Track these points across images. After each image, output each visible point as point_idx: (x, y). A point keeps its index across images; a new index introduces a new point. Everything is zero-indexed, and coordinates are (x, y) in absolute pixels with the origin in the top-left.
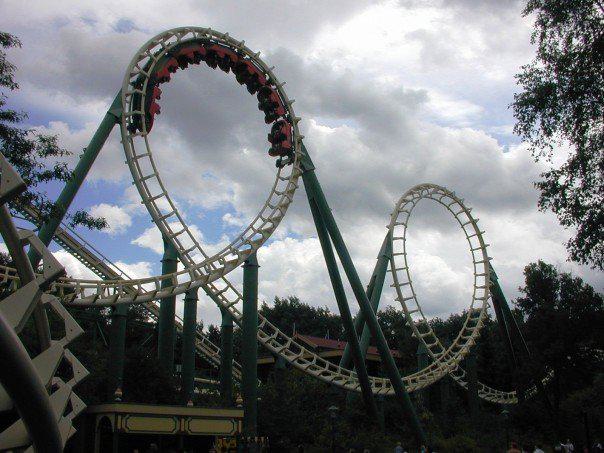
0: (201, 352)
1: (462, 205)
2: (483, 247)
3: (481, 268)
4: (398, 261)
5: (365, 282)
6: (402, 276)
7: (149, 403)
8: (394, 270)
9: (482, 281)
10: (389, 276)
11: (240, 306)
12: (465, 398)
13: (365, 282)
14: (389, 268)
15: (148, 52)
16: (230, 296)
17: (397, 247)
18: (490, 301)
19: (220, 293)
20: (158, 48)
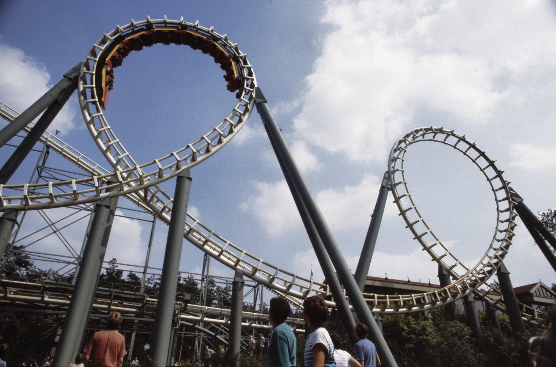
17: (397, 178)
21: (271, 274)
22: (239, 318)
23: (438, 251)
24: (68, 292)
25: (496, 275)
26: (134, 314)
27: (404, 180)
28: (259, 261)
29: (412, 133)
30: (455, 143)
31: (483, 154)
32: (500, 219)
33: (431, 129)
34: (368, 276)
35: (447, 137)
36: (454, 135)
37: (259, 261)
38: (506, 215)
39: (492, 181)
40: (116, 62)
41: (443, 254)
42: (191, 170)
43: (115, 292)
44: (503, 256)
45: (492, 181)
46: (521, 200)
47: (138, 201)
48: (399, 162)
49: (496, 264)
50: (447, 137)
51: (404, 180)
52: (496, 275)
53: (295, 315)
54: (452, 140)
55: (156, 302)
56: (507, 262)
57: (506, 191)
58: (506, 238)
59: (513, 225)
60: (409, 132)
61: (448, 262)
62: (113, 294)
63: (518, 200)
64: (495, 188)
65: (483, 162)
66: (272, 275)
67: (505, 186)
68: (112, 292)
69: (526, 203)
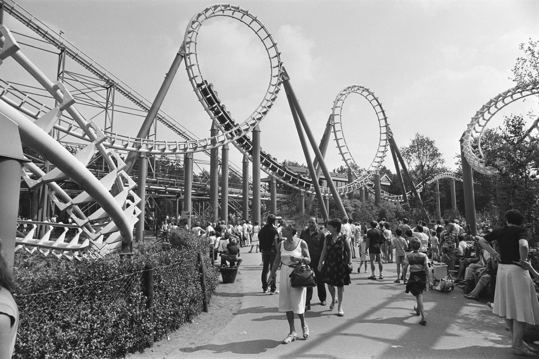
3: (384, 130)
4: (338, 127)
8: (335, 132)
9: (384, 137)
10: (332, 136)
14: (332, 130)
17: (337, 119)
22: (227, 192)
24: (437, 178)
28: (42, 105)
29: (358, 86)
31: (383, 112)
35: (368, 95)
36: (377, 101)
37: (42, 105)
38: (383, 149)
44: (259, 119)
46: (288, 79)
47: (28, 21)
48: (344, 96)
49: (253, 125)
50: (368, 95)
53: (527, 177)
55: (183, 182)
56: (262, 126)
57: (387, 128)
58: (266, 106)
59: (385, 155)
60: (356, 85)
65: (381, 116)
67: (387, 126)
69: (291, 82)
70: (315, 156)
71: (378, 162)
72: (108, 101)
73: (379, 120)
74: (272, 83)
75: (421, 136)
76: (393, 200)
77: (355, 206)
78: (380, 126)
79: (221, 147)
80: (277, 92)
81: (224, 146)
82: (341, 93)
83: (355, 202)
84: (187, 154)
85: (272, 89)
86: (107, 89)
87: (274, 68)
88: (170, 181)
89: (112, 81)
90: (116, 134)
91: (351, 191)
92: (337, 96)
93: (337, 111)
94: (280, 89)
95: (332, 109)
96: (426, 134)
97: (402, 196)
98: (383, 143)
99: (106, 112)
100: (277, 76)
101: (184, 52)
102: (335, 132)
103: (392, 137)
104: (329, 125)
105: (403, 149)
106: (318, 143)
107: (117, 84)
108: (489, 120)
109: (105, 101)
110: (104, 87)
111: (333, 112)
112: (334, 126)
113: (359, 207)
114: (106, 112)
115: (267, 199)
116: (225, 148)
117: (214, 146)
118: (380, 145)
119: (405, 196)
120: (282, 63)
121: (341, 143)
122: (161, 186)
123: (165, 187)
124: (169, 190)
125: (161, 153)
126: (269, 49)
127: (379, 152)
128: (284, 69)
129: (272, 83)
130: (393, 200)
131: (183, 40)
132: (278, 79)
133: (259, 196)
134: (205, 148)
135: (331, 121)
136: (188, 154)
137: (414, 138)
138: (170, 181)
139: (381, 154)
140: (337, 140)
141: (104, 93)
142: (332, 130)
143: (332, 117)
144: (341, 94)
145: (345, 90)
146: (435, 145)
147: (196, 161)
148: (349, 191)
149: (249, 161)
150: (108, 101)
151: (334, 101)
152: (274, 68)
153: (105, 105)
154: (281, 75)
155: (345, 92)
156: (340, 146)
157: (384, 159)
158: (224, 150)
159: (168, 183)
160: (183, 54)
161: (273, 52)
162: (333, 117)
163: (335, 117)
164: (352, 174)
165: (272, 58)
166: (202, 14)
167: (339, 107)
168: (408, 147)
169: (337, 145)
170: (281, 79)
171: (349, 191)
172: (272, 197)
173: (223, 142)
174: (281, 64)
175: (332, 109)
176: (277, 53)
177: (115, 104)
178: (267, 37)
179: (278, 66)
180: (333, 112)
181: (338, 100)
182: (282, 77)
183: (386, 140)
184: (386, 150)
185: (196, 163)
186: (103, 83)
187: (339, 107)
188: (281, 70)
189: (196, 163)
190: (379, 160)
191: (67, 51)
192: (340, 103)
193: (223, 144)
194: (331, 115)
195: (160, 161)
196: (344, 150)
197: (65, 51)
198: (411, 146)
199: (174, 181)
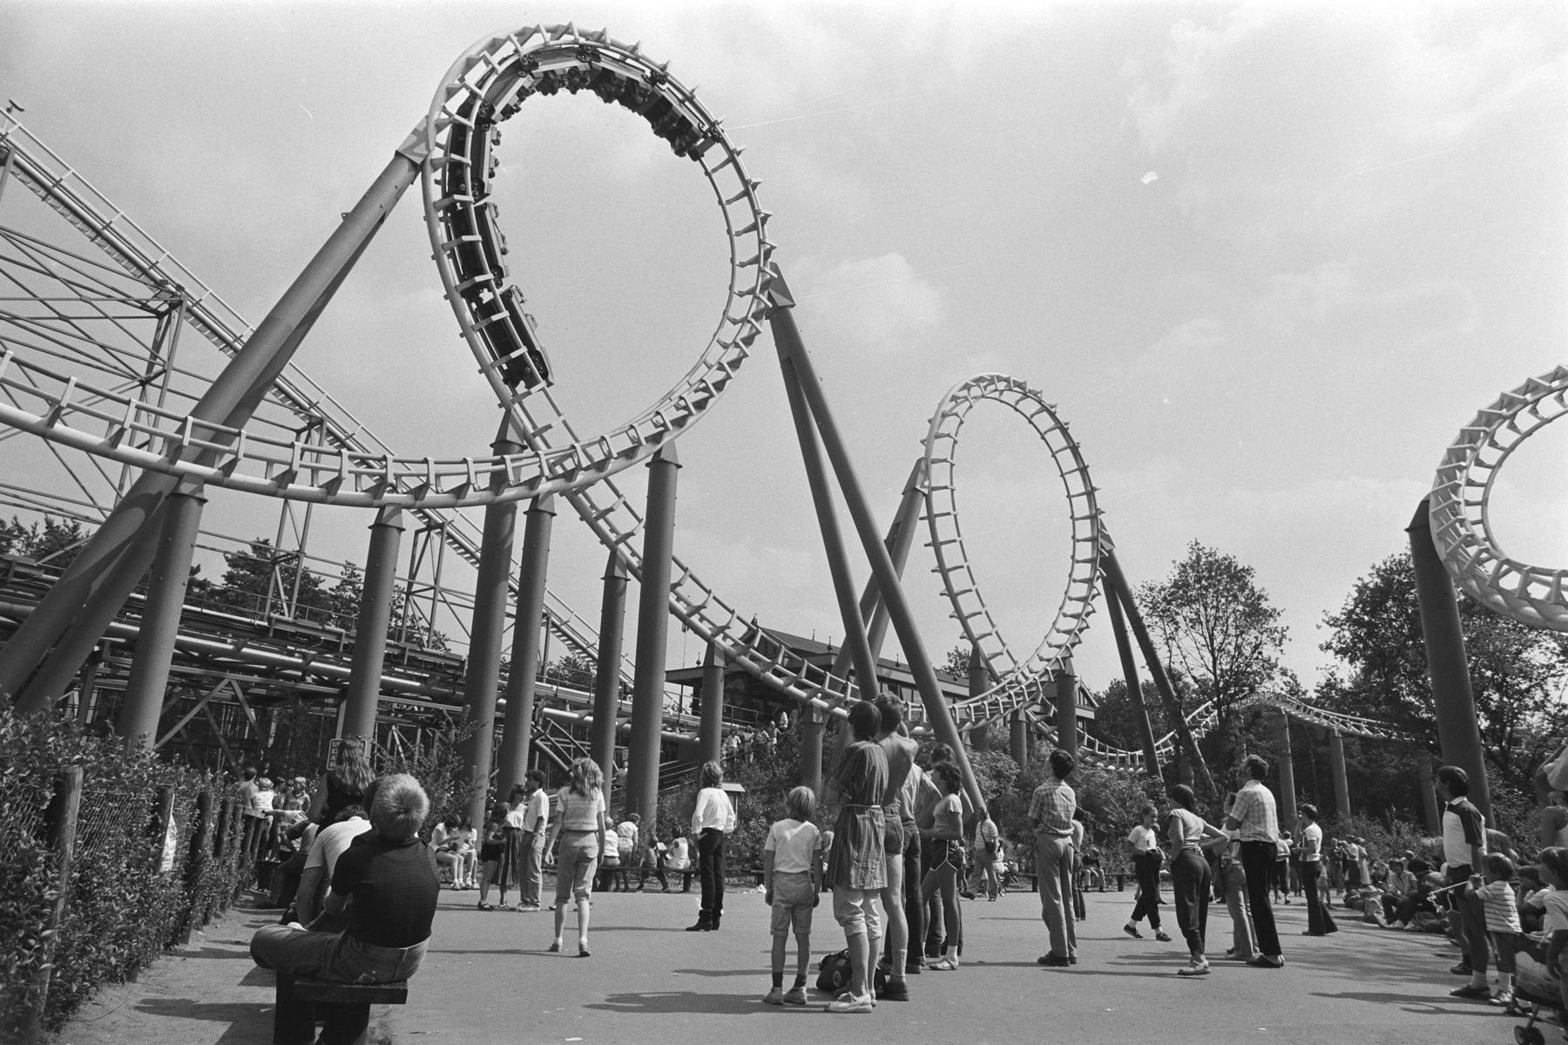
0: (1369, 944)
1: (1053, 415)
2: (1090, 493)
3: (1085, 530)
4: (940, 502)
5: (883, 527)
6: (945, 529)
7: (557, 709)
8: (931, 518)
9: (1085, 550)
10: (921, 531)
11: (638, 543)
12: (197, 720)
13: (883, 527)
14: (923, 512)
15: (462, 79)
16: (622, 521)
17: (939, 475)
18: (1099, 584)
19: (603, 514)
20: (480, 70)
21: (117, 418)
23: (978, 626)
25: (647, 465)
26: (417, 681)
27: (952, 484)
30: (1046, 429)
31: (1083, 470)
32: (1070, 594)
33: (1020, 385)
34: (881, 656)
38: (1082, 590)
39: (1076, 522)
40: (548, 85)
41: (987, 632)
42: (676, 440)
43: (410, 650)
45: (1076, 522)
50: (1021, 399)
51: (952, 484)
52: (647, 465)
54: (1030, 406)
56: (684, 446)
59: (1089, 609)
61: (987, 647)
62: (407, 653)
63: (781, 301)
64: (1078, 537)
66: (119, 422)
67: (1094, 517)
68: (404, 649)
70: (869, 571)
71: (1068, 632)
72: (154, 356)
73: (1069, 496)
74: (731, 314)
75: (1206, 551)
76: (1112, 767)
77: (998, 775)
78: (1072, 517)
79: (524, 506)
80: (749, 341)
81: (535, 499)
82: (954, 392)
83: (995, 760)
84: (382, 508)
85: (730, 333)
86: (159, 315)
87: (743, 265)
88: (324, 631)
89: (179, 288)
90: (74, 379)
91: (983, 722)
92: (940, 405)
93: (941, 448)
94: (758, 332)
95: (922, 442)
96: (1226, 545)
97: (1140, 753)
98: (1084, 571)
99: (144, 389)
100: (752, 292)
101: (426, 152)
102: (931, 518)
103: (1110, 552)
104: (911, 493)
105: (1151, 589)
106: (883, 528)
107: (197, 303)
108: (1529, 433)
109: (147, 355)
110: (144, 307)
111: (928, 452)
112: (928, 498)
113: (1008, 779)
114: (144, 389)
115: (686, 736)
116: (541, 508)
117: (497, 495)
118: (1074, 576)
119: (1149, 751)
120: (773, 248)
121: (951, 555)
122: (291, 654)
123: (304, 656)
124: (317, 672)
125: (273, 489)
126: (729, 202)
127: (1071, 599)
128: (775, 268)
129: (731, 314)
130: (1112, 767)
131: (427, 112)
132: (761, 270)
133: (659, 724)
134: (458, 497)
135: (920, 476)
136: (388, 510)
137: (1185, 556)
138: (324, 631)
139: (1077, 607)
140: (936, 544)
141: (147, 328)
142: (923, 512)
143: (922, 468)
144: (954, 398)
145: (967, 387)
146: (1257, 582)
147: (450, 598)
148: (978, 720)
149: (630, 575)
150: (154, 356)
151: (931, 417)
152: (743, 265)
153: (143, 372)
154: (763, 288)
155: (965, 393)
156: (948, 565)
157: (1089, 619)
158: (537, 517)
159: (311, 641)
160: (420, 155)
161: (741, 214)
162: (927, 467)
163: (934, 467)
164: (983, 665)
165: (738, 234)
166: (505, 41)
167: (949, 435)
168: (1168, 585)
169: (935, 564)
170: (764, 298)
171: (978, 720)
172: (706, 730)
173: (532, 483)
174: (768, 254)
175: (922, 442)
176: (756, 213)
177: (175, 365)
178: (727, 162)
179: (756, 260)
180: (928, 452)
181: (944, 415)
182: (769, 293)
183: (1092, 561)
184: (1095, 592)
185: (449, 604)
186: (143, 292)
187: (949, 435)
188: (768, 270)
189: (449, 604)
190: (1072, 624)
191: (16, 163)
192: (949, 425)
193: (534, 493)
194: (919, 461)
195: (336, 597)
196: (959, 580)
197: (10, 162)
198: (1175, 585)
199: (339, 635)
